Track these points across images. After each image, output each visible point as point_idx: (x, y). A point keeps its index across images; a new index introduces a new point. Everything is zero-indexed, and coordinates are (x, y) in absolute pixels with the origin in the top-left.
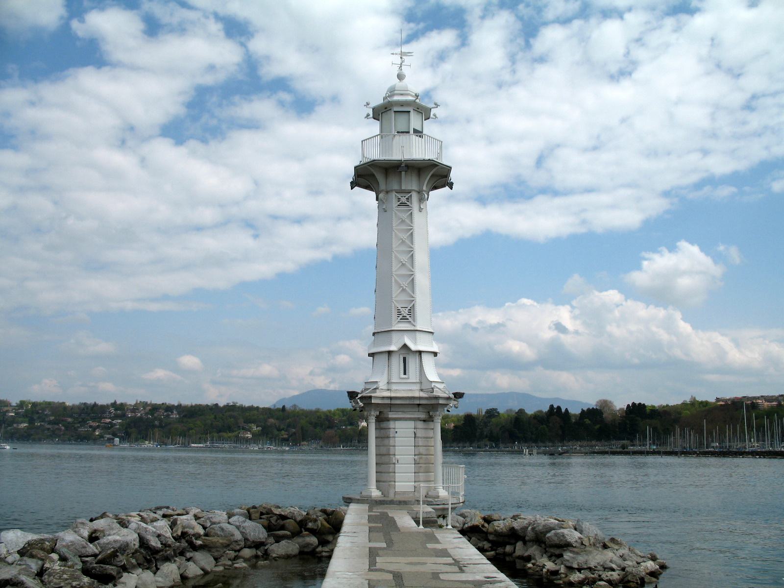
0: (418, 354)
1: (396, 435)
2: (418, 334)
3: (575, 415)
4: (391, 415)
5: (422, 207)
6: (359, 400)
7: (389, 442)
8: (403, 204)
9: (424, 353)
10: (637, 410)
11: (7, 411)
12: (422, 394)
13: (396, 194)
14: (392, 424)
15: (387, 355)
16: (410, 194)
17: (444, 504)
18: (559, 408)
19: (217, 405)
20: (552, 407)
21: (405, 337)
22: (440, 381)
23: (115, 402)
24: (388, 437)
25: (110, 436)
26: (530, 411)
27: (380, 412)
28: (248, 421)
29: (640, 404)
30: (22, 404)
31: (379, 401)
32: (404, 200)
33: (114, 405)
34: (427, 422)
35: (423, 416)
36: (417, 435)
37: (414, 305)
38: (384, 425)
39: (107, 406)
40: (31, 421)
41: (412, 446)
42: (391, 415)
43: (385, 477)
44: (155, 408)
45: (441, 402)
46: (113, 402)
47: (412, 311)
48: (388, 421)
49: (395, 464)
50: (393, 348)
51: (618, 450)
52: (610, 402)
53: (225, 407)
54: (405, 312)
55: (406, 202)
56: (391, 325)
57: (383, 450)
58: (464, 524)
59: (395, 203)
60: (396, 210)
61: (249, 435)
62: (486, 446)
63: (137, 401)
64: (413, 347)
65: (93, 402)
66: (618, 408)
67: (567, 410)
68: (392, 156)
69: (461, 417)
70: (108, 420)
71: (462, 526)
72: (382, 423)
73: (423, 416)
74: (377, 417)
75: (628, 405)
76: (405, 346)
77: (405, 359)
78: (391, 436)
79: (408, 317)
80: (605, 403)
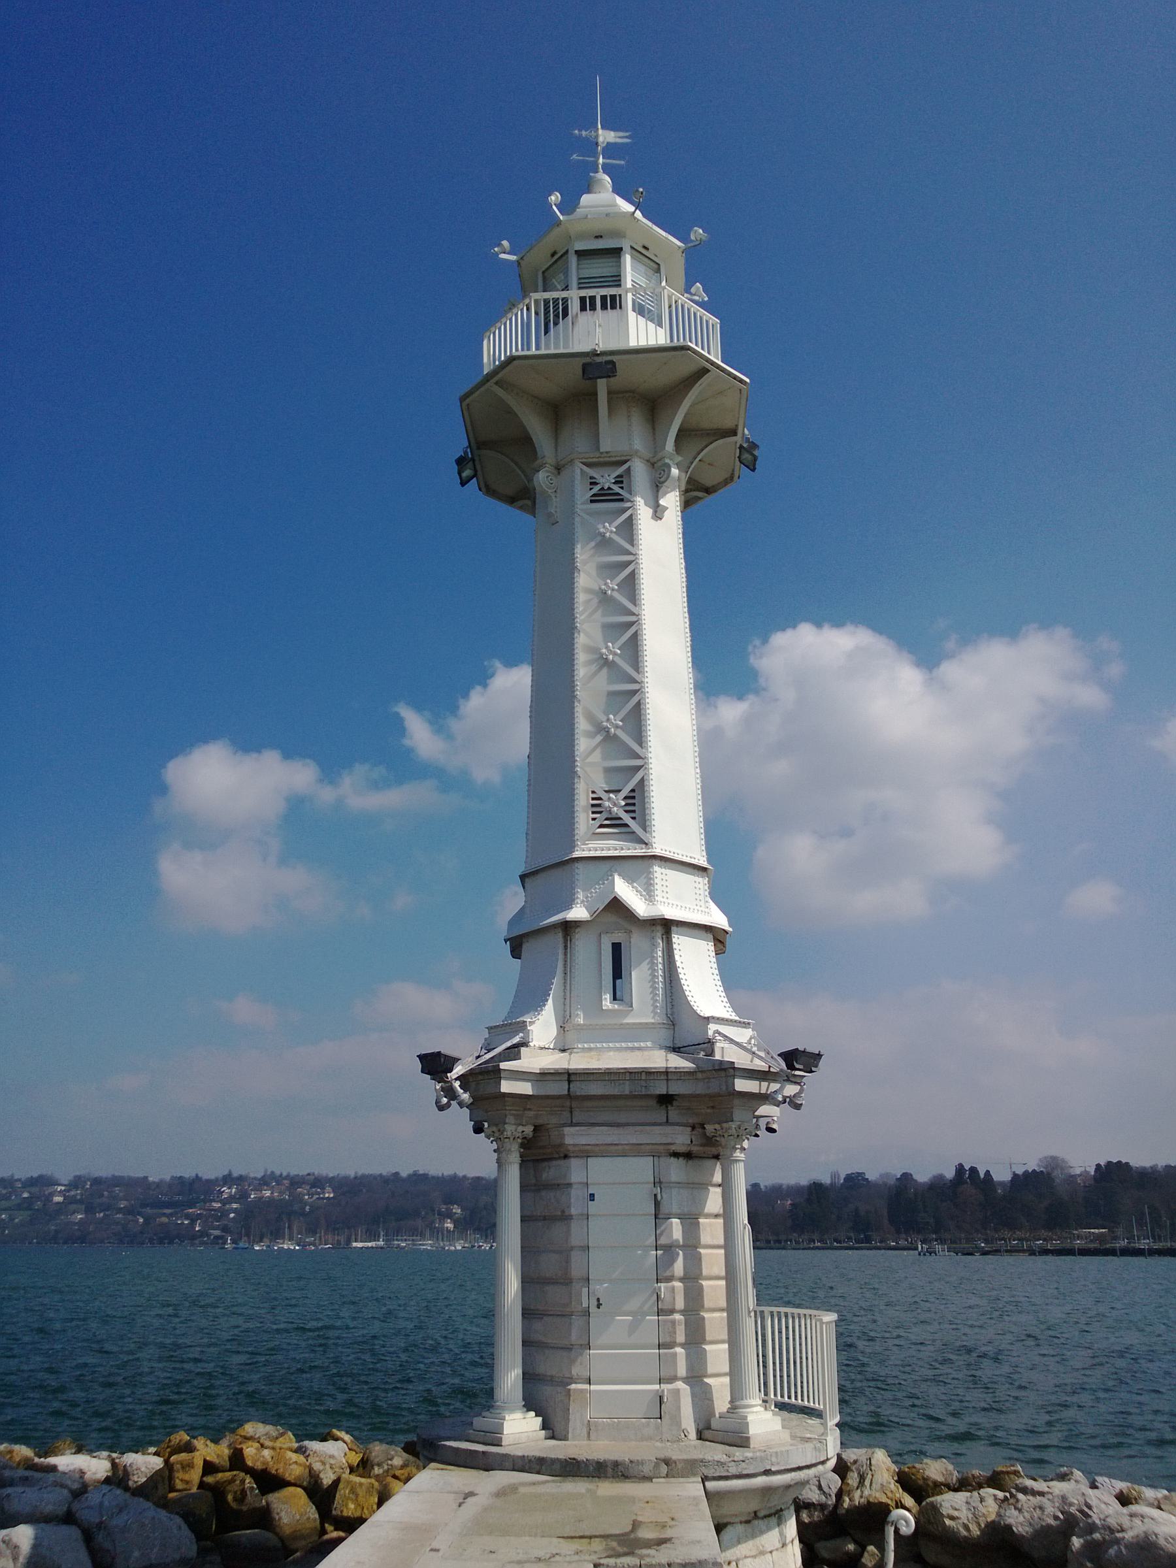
0: (659, 931)
1: (593, 1207)
2: (658, 871)
3: (1001, 1184)
4: (573, 1137)
5: (662, 502)
6: (457, 1084)
7: (568, 1232)
8: (602, 496)
9: (680, 929)
10: (1113, 1175)
11: (52, 1195)
12: (677, 1062)
13: (585, 468)
14: (576, 1171)
15: (560, 935)
16: (626, 466)
17: (767, 1472)
18: (973, 1170)
19: (397, 1174)
20: (960, 1169)
21: (617, 878)
22: (734, 1017)
23: (230, 1174)
24: (565, 1218)
25: (217, 1233)
26: (922, 1176)
27: (537, 1128)
28: (449, 1200)
29: (1109, 1163)
30: (77, 1182)
31: (526, 1088)
32: (607, 479)
33: (228, 1180)
34: (696, 1162)
35: (681, 1138)
36: (664, 1209)
37: (642, 780)
38: (550, 1173)
39: (215, 1182)
40: (90, 1210)
41: (718, 1247)
42: (573, 1137)
43: (548, 1365)
44: (295, 1182)
45: (741, 1085)
46: (226, 1173)
47: (637, 801)
48: (566, 1157)
49: (587, 1313)
50: (578, 913)
51: (1092, 1246)
52: (1063, 1161)
53: (410, 1176)
54: (616, 805)
55: (616, 489)
56: (572, 847)
57: (548, 1265)
58: (840, 1495)
59: (582, 494)
60: (590, 514)
61: (449, 1225)
62: (850, 1239)
63: (266, 1170)
64: (640, 907)
65: (194, 1175)
66: (1078, 1171)
67: (988, 1172)
68: (566, 346)
69: (803, 1187)
70: (217, 1205)
71: (832, 1501)
72: (545, 1164)
73: (681, 1138)
74: (527, 1144)
75: (1098, 1166)
76: (616, 906)
77: (617, 948)
78: (573, 1211)
79: (626, 818)
80: (1054, 1163)
